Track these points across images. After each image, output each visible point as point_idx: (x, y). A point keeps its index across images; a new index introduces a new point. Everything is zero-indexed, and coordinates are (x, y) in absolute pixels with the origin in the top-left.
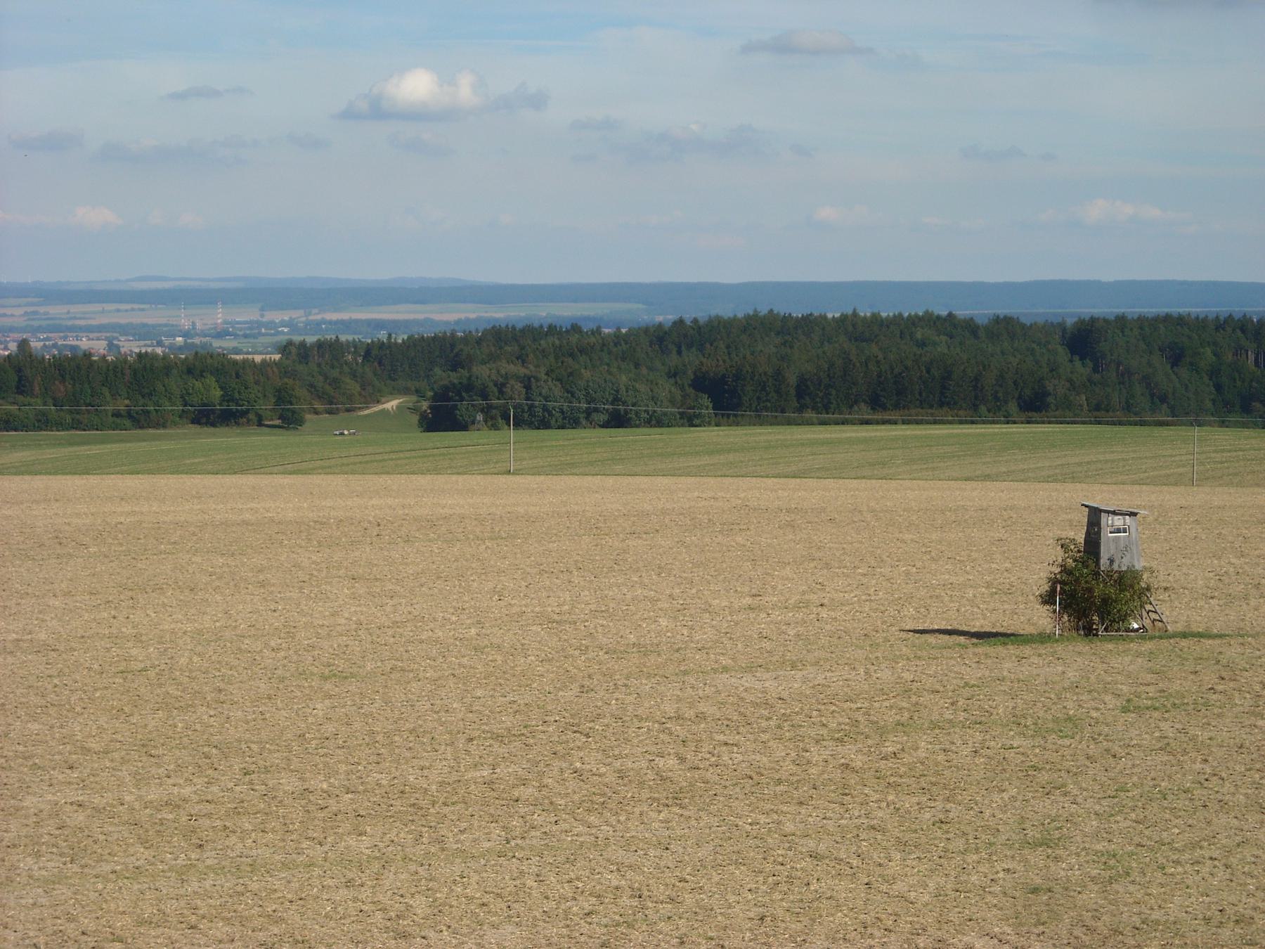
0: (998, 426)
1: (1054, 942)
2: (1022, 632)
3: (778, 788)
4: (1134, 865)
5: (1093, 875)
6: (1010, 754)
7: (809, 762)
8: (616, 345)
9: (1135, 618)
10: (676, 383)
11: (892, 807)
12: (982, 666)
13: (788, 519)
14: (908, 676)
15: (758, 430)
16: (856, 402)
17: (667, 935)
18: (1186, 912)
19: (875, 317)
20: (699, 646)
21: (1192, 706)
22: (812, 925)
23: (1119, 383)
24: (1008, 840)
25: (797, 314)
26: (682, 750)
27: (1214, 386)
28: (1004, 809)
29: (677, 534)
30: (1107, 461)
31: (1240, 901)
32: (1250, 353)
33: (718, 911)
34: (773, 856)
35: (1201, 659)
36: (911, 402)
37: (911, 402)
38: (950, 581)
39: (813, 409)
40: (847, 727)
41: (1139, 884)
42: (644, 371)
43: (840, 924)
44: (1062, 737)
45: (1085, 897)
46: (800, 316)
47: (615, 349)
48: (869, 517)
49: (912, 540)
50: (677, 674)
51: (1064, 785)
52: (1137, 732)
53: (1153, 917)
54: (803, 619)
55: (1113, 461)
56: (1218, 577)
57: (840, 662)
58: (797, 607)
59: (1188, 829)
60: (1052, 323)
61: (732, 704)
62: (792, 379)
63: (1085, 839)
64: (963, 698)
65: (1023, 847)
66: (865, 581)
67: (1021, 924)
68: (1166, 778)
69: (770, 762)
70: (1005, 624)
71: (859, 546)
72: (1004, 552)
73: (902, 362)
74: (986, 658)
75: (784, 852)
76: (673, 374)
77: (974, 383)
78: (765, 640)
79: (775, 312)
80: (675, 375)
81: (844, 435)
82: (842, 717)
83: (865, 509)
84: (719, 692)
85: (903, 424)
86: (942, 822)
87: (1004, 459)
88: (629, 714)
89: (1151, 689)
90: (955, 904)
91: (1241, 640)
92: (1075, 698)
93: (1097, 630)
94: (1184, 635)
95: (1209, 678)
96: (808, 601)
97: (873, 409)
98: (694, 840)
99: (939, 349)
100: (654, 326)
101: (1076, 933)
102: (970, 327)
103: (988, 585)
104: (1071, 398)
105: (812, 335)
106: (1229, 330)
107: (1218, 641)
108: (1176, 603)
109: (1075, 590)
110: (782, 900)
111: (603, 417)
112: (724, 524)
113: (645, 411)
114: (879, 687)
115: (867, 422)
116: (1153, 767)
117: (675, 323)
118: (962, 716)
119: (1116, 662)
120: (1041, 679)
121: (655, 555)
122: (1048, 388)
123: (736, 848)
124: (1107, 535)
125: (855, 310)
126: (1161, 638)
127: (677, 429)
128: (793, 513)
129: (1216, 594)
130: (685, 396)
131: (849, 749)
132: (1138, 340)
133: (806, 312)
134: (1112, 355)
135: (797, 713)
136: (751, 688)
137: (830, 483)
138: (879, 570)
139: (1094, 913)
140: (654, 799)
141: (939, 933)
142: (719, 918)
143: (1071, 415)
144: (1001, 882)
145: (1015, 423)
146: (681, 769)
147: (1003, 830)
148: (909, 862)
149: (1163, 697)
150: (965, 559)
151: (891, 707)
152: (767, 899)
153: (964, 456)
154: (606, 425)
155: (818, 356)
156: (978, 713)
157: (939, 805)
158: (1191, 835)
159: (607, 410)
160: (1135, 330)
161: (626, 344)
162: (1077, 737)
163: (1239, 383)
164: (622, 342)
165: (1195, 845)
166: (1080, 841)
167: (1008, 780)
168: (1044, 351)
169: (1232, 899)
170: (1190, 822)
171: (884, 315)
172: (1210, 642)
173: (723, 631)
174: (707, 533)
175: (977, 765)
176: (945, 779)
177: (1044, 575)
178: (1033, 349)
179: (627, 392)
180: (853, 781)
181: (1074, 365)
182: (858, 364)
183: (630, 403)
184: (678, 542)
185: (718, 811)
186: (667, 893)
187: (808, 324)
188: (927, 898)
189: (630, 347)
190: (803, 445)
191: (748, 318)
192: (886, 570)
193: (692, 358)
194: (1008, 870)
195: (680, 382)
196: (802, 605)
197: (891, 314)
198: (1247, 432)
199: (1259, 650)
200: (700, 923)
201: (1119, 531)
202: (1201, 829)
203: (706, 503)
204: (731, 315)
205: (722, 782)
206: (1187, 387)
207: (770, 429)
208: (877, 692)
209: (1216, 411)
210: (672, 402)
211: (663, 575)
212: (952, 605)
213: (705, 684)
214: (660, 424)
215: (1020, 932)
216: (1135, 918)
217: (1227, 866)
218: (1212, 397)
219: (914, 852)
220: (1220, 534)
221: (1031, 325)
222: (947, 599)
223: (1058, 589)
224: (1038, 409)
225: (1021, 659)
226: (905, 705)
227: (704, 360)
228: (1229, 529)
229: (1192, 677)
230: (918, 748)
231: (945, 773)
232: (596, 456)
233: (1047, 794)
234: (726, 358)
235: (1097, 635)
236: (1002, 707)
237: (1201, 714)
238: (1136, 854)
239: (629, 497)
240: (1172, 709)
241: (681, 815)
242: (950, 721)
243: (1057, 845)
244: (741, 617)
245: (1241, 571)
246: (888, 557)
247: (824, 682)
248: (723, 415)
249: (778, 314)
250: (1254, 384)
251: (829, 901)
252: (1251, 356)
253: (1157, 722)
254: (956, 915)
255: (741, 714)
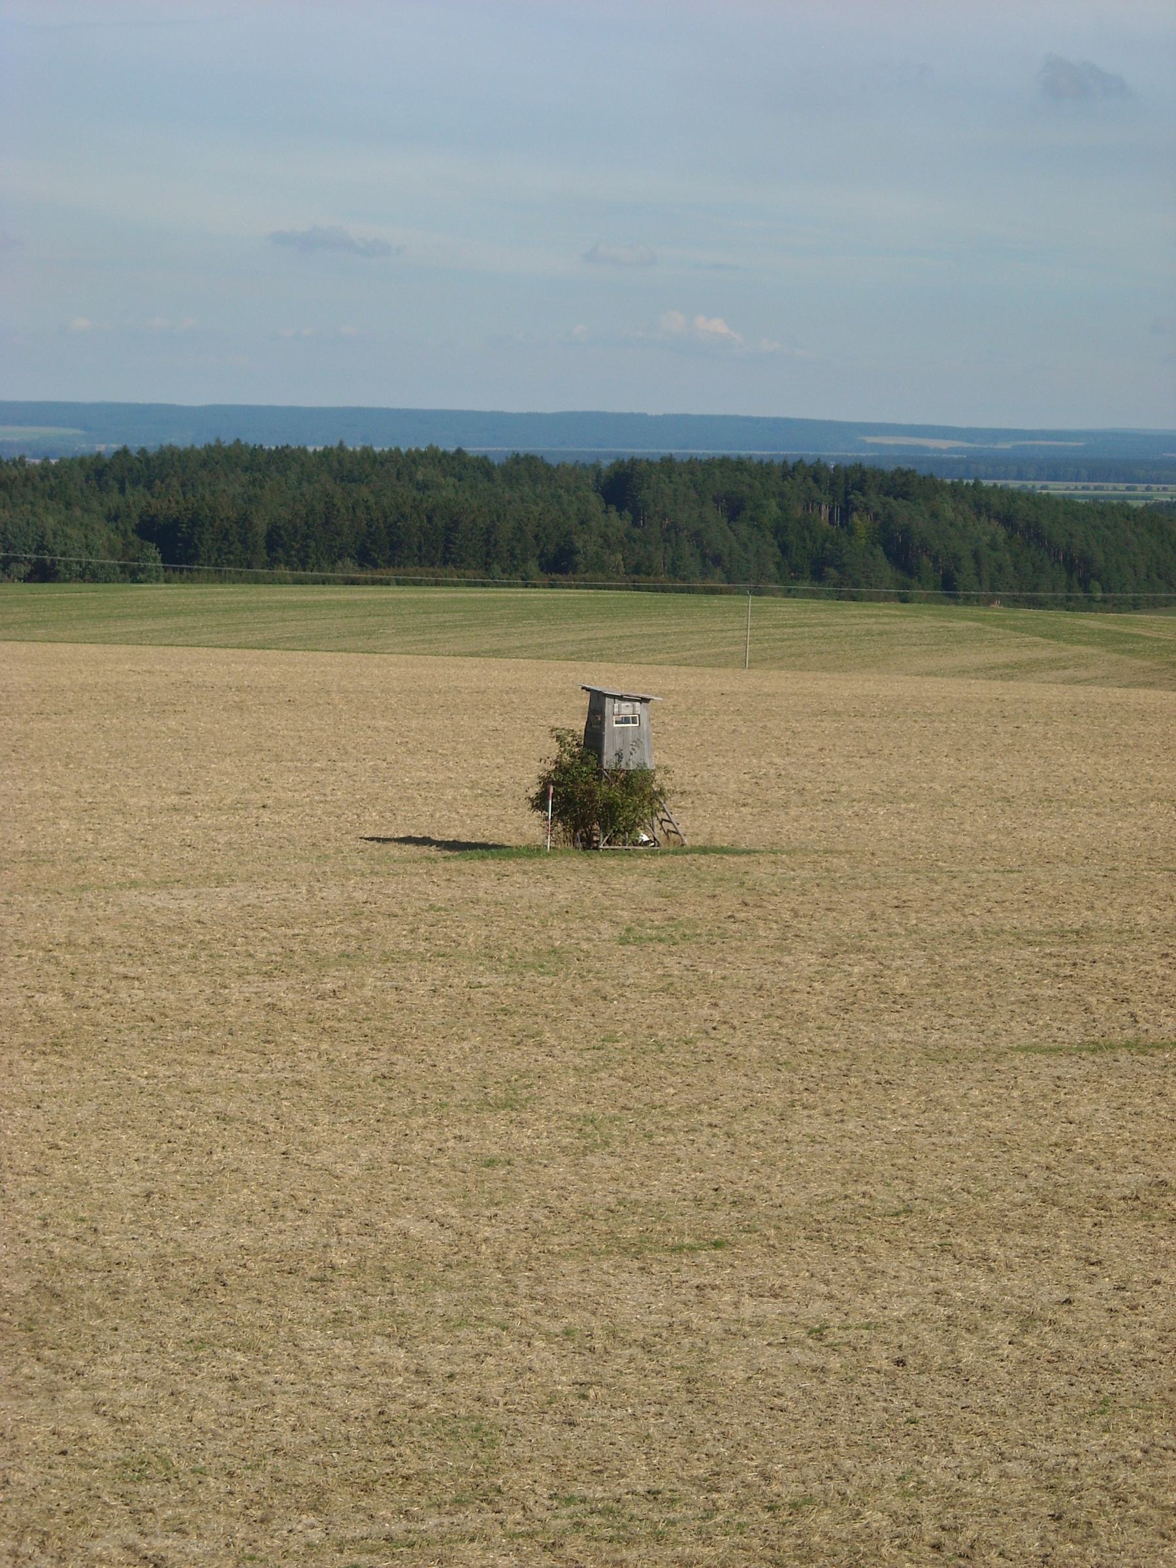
0: (513, 590)
1: (509, 1227)
2: (507, 844)
3: (185, 1033)
4: (616, 1133)
5: (564, 1144)
6: (477, 994)
7: (227, 1001)
8: (42, 478)
9: (644, 829)
10: (117, 528)
11: (325, 1059)
12: (453, 885)
13: (237, 699)
14: (360, 896)
15: (219, 588)
16: (340, 557)
17: (27, 1215)
18: (674, 1191)
19: (367, 453)
20: (105, 855)
21: (706, 938)
22: (210, 1205)
23: (665, 541)
24: (465, 1100)
25: (270, 445)
26: (69, 984)
27: (779, 546)
28: (463, 1062)
29: (95, 715)
30: (643, 636)
31: (740, 1178)
32: (823, 507)
33: (95, 1185)
34: (170, 1117)
35: (722, 880)
36: (408, 558)
37: (408, 558)
38: (427, 780)
39: (287, 563)
40: (278, 959)
41: (620, 1156)
42: (78, 512)
43: (245, 1204)
44: (542, 974)
45: (552, 1171)
46: (273, 448)
47: (41, 485)
48: (336, 697)
49: (386, 728)
50: (73, 890)
51: (539, 1033)
52: (636, 969)
53: (633, 1196)
54: (238, 824)
55: (650, 636)
56: (754, 780)
57: (277, 877)
58: (233, 808)
59: (686, 1088)
60: (584, 465)
61: (139, 928)
62: (261, 526)
63: (559, 1100)
64: (425, 924)
65: (482, 1109)
66: (321, 777)
67: (469, 1205)
68: (665, 1027)
69: (178, 1000)
70: (487, 833)
71: (320, 734)
72: (498, 745)
73: (398, 508)
74: (459, 875)
75: (184, 1113)
76: (113, 517)
77: (486, 536)
78: (188, 849)
79: (243, 443)
80: (116, 519)
81: (323, 598)
82: (273, 945)
83: (335, 689)
84: (123, 913)
85: (398, 584)
86: (385, 1077)
87: (519, 631)
88: (8, 938)
89: (657, 916)
90: (390, 1179)
91: (773, 858)
92: (564, 926)
93: (597, 842)
94: (704, 850)
95: (729, 903)
96: (249, 802)
97: (361, 565)
98: (74, 1097)
99: (444, 494)
100: (91, 456)
101: (535, 1216)
102: (483, 466)
103: (473, 785)
104: (605, 557)
105: (288, 472)
106: (799, 479)
107: (744, 859)
108: (700, 812)
109: (572, 792)
110: (176, 1172)
111: (24, 569)
112: (157, 704)
113: (78, 562)
114: (323, 908)
115: (353, 582)
116: (651, 1012)
117: (117, 453)
118: (422, 946)
119: (617, 883)
120: (524, 902)
121: (64, 741)
122: (577, 544)
123: (125, 1108)
124: (612, 725)
125: (341, 443)
126: (675, 853)
127: (116, 585)
128: (245, 692)
129: (750, 801)
130: (129, 544)
131: (279, 986)
132: (689, 488)
133: (281, 443)
134: (656, 506)
135: (218, 940)
136: (164, 908)
137: (299, 656)
138: (340, 764)
139: (561, 1191)
140: (28, 1045)
141: (367, 1215)
142: (96, 1194)
143: (604, 578)
144: (450, 1152)
145: (535, 586)
146: (66, 1008)
147: (459, 1088)
148: (339, 1127)
149: (671, 926)
150: (449, 753)
151: (336, 933)
152: (157, 1171)
153: (470, 626)
154: (28, 579)
155: (294, 498)
156: (442, 942)
157: (383, 1055)
158: (690, 1097)
159: (30, 561)
160: (684, 475)
161: (56, 478)
162: (562, 975)
163: (809, 544)
164: (50, 475)
165: (693, 1109)
166: (553, 1103)
167: (471, 1026)
168: (573, 498)
169: (732, 1175)
170: (689, 1080)
171: (377, 449)
172: (735, 859)
173: (137, 837)
174: (134, 714)
175: (434, 1007)
176: (394, 1024)
177: (533, 777)
178: (560, 497)
179: (55, 538)
180: (279, 1026)
181: (609, 517)
182: (343, 510)
183: (58, 552)
184: (95, 725)
185: (107, 1061)
186: (33, 1163)
187: (283, 458)
188: (356, 1171)
189: (60, 482)
190: (271, 608)
191: (209, 449)
192: (349, 765)
193: (137, 498)
194: (461, 1137)
195: (121, 527)
196: (239, 806)
197: (386, 449)
198: (814, 604)
199: (794, 870)
200: (71, 1201)
201: (626, 720)
202: (702, 1088)
203: (139, 678)
204: (188, 445)
205: (116, 1024)
206: (745, 545)
207: (231, 588)
208: (320, 916)
209: (781, 578)
210: (112, 552)
211: (71, 766)
212: (425, 809)
213: (107, 903)
214: (95, 578)
215: (466, 1215)
216: (611, 1199)
217: (728, 1135)
218: (777, 559)
219: (347, 1114)
220: (765, 727)
221: (558, 465)
222: (420, 800)
223: (551, 791)
224: (563, 571)
225: (501, 876)
226: (353, 931)
227: (153, 501)
228: (776, 721)
229: (709, 902)
230: (363, 985)
231: (392, 1016)
232: (12, 617)
233: (518, 1044)
234: (181, 499)
235: (597, 849)
236: (473, 935)
237: (715, 947)
238: (620, 1119)
239: (44, 669)
240: (680, 941)
241: (61, 1066)
242: (408, 952)
243: (524, 1107)
244: (162, 819)
245: (783, 773)
246: (354, 748)
247: (255, 902)
248: (174, 570)
249: (246, 446)
250: (828, 545)
251: (234, 1174)
252: (825, 511)
253: (661, 956)
254: (390, 1193)
255: (148, 940)
